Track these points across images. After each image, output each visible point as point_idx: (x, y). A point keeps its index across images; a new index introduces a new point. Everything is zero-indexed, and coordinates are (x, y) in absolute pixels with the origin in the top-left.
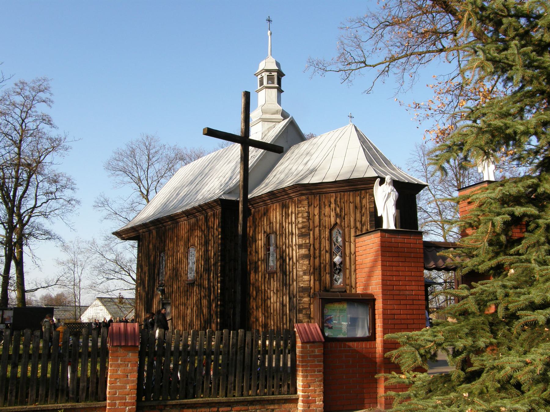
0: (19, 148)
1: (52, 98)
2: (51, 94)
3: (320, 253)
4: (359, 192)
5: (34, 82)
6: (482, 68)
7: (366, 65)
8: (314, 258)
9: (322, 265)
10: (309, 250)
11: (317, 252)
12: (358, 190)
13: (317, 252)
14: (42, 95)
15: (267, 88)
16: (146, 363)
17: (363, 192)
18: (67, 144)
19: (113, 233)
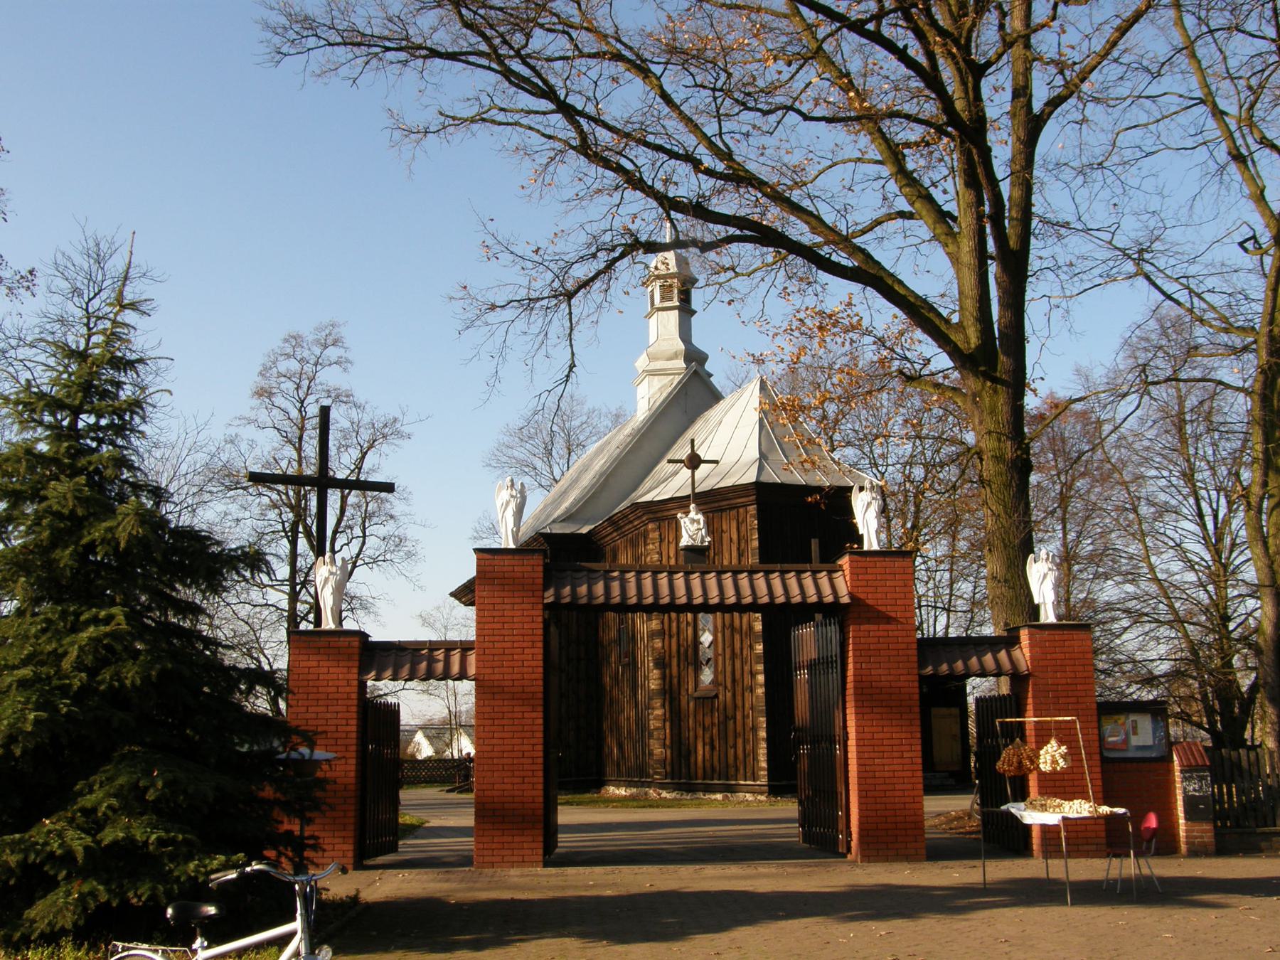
0: (299, 450)
1: (350, 356)
2: (346, 349)
3: (678, 627)
4: (734, 512)
5: (319, 329)
6: (158, 473)
7: (737, 275)
8: (670, 637)
9: (682, 649)
10: (662, 623)
11: (674, 625)
12: (731, 509)
13: (674, 625)
14: (333, 353)
15: (659, 309)
16: (1115, 810)
17: (741, 510)
18: (406, 429)
19: (452, 594)
